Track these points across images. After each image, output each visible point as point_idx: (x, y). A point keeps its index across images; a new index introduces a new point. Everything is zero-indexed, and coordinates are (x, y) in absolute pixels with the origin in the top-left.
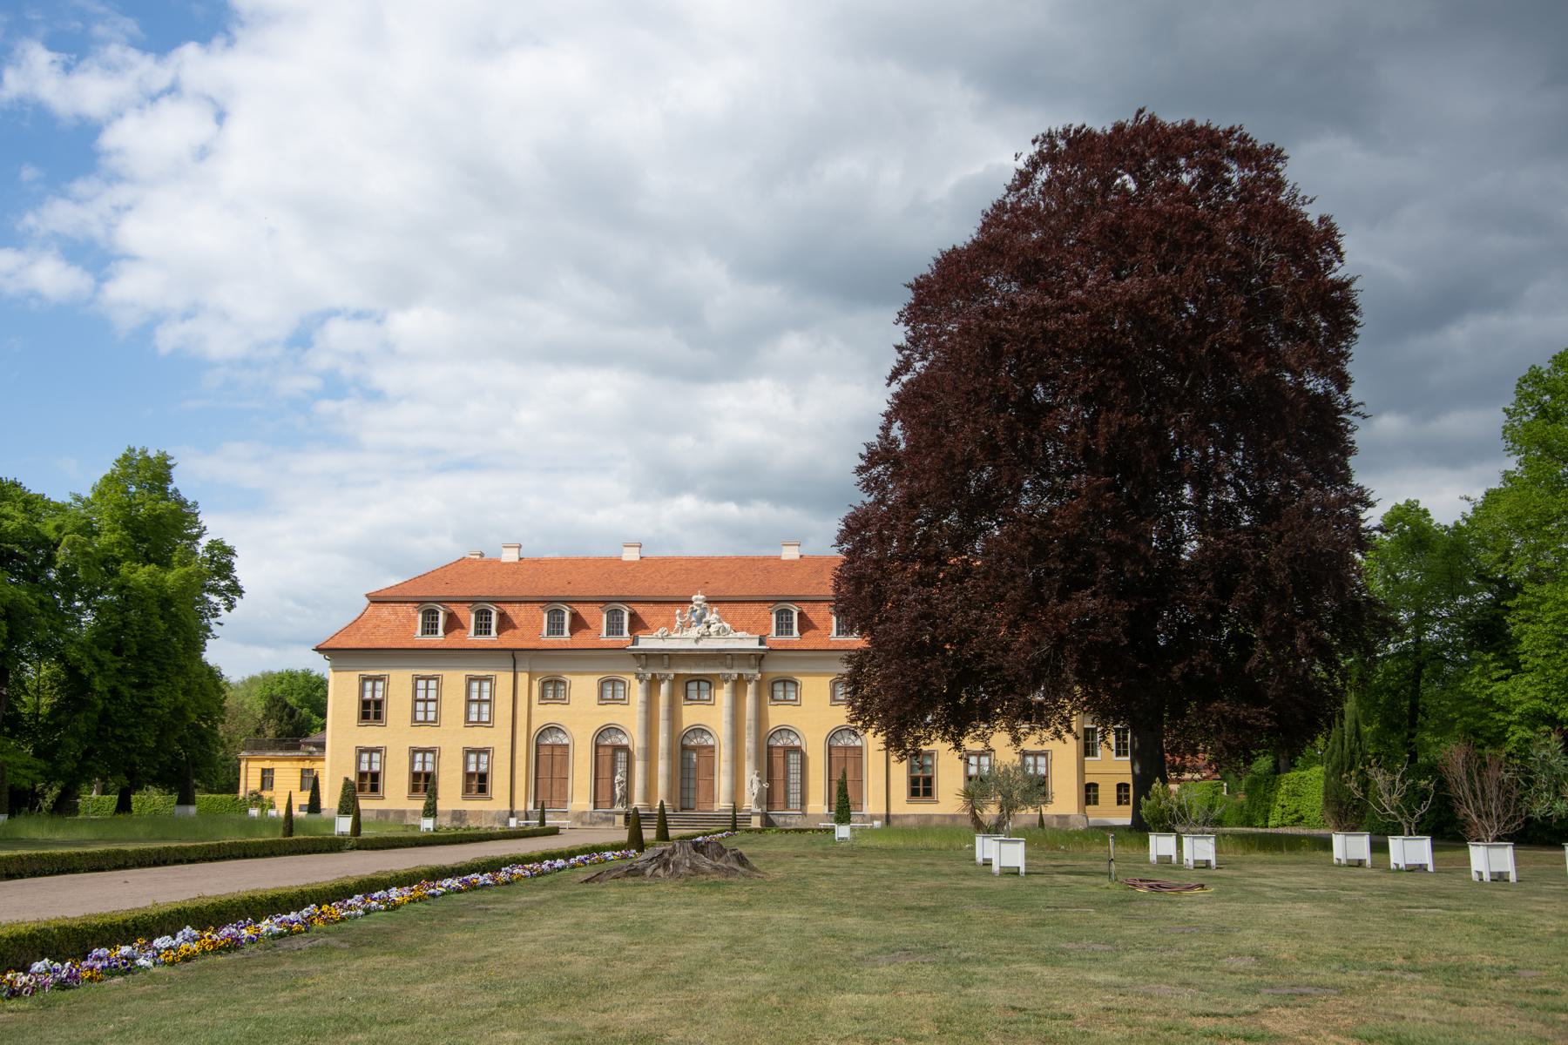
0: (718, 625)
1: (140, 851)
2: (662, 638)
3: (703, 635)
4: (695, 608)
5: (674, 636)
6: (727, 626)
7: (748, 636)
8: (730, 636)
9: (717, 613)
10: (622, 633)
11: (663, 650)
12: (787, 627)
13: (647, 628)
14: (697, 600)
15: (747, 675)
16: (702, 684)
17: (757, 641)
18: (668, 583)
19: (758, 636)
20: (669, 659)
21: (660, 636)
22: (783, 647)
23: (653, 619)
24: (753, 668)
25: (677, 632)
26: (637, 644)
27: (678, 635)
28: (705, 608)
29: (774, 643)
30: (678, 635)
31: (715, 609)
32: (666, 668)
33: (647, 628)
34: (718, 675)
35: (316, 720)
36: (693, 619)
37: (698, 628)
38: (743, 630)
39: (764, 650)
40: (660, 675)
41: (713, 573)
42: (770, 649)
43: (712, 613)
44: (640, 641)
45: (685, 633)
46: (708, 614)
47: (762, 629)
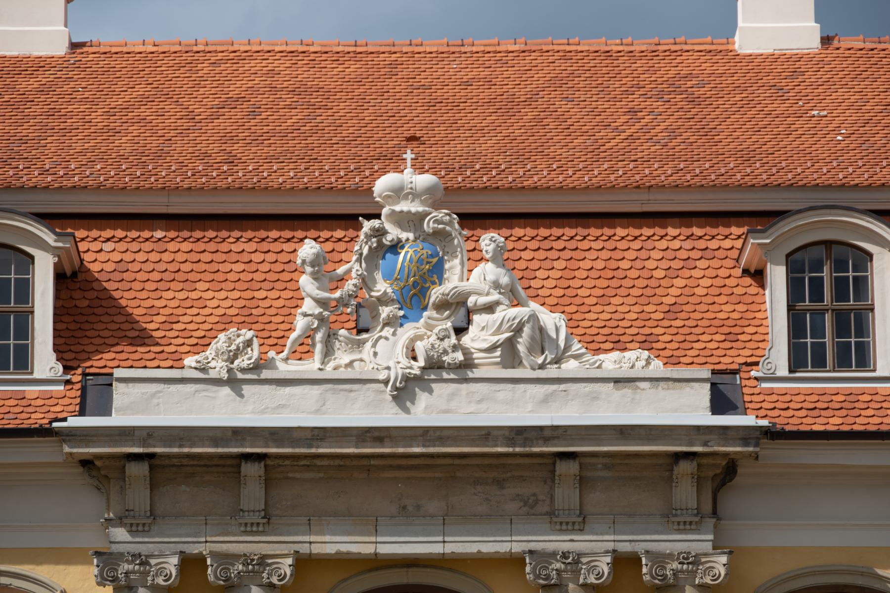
0: (507, 313)
1: (321, 535)
2: (232, 382)
3: (434, 365)
4: (394, 233)
5: (286, 368)
6: (551, 320)
7: (657, 367)
8: (570, 367)
9: (500, 258)
10: (23, 361)
11: (238, 433)
12: (842, 329)
13: (142, 338)
14: (398, 193)
15: (659, 559)
16: (696, 511)
17: (704, 393)
18: (229, 138)
19: (705, 373)
20: (268, 482)
21: (219, 369)
22: (834, 423)
23: (172, 298)
24: (686, 527)
25: (303, 351)
26: (106, 411)
27: (311, 367)
28: (440, 236)
29: (786, 402)
30: (311, 367)
31: (489, 241)
32: (250, 529)
33: (142, 338)
34: (515, 562)
35: (315, 277)
36: (382, 287)
37: (408, 331)
38: (620, 345)
39: (746, 435)
40: (225, 559)
41: (432, 105)
42: (772, 434)
43: (475, 257)
44: (121, 394)
45: (343, 357)
46: (454, 267)
47: (711, 341)
